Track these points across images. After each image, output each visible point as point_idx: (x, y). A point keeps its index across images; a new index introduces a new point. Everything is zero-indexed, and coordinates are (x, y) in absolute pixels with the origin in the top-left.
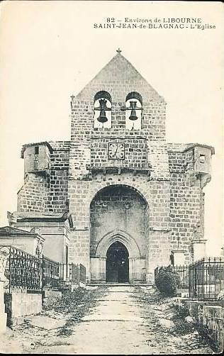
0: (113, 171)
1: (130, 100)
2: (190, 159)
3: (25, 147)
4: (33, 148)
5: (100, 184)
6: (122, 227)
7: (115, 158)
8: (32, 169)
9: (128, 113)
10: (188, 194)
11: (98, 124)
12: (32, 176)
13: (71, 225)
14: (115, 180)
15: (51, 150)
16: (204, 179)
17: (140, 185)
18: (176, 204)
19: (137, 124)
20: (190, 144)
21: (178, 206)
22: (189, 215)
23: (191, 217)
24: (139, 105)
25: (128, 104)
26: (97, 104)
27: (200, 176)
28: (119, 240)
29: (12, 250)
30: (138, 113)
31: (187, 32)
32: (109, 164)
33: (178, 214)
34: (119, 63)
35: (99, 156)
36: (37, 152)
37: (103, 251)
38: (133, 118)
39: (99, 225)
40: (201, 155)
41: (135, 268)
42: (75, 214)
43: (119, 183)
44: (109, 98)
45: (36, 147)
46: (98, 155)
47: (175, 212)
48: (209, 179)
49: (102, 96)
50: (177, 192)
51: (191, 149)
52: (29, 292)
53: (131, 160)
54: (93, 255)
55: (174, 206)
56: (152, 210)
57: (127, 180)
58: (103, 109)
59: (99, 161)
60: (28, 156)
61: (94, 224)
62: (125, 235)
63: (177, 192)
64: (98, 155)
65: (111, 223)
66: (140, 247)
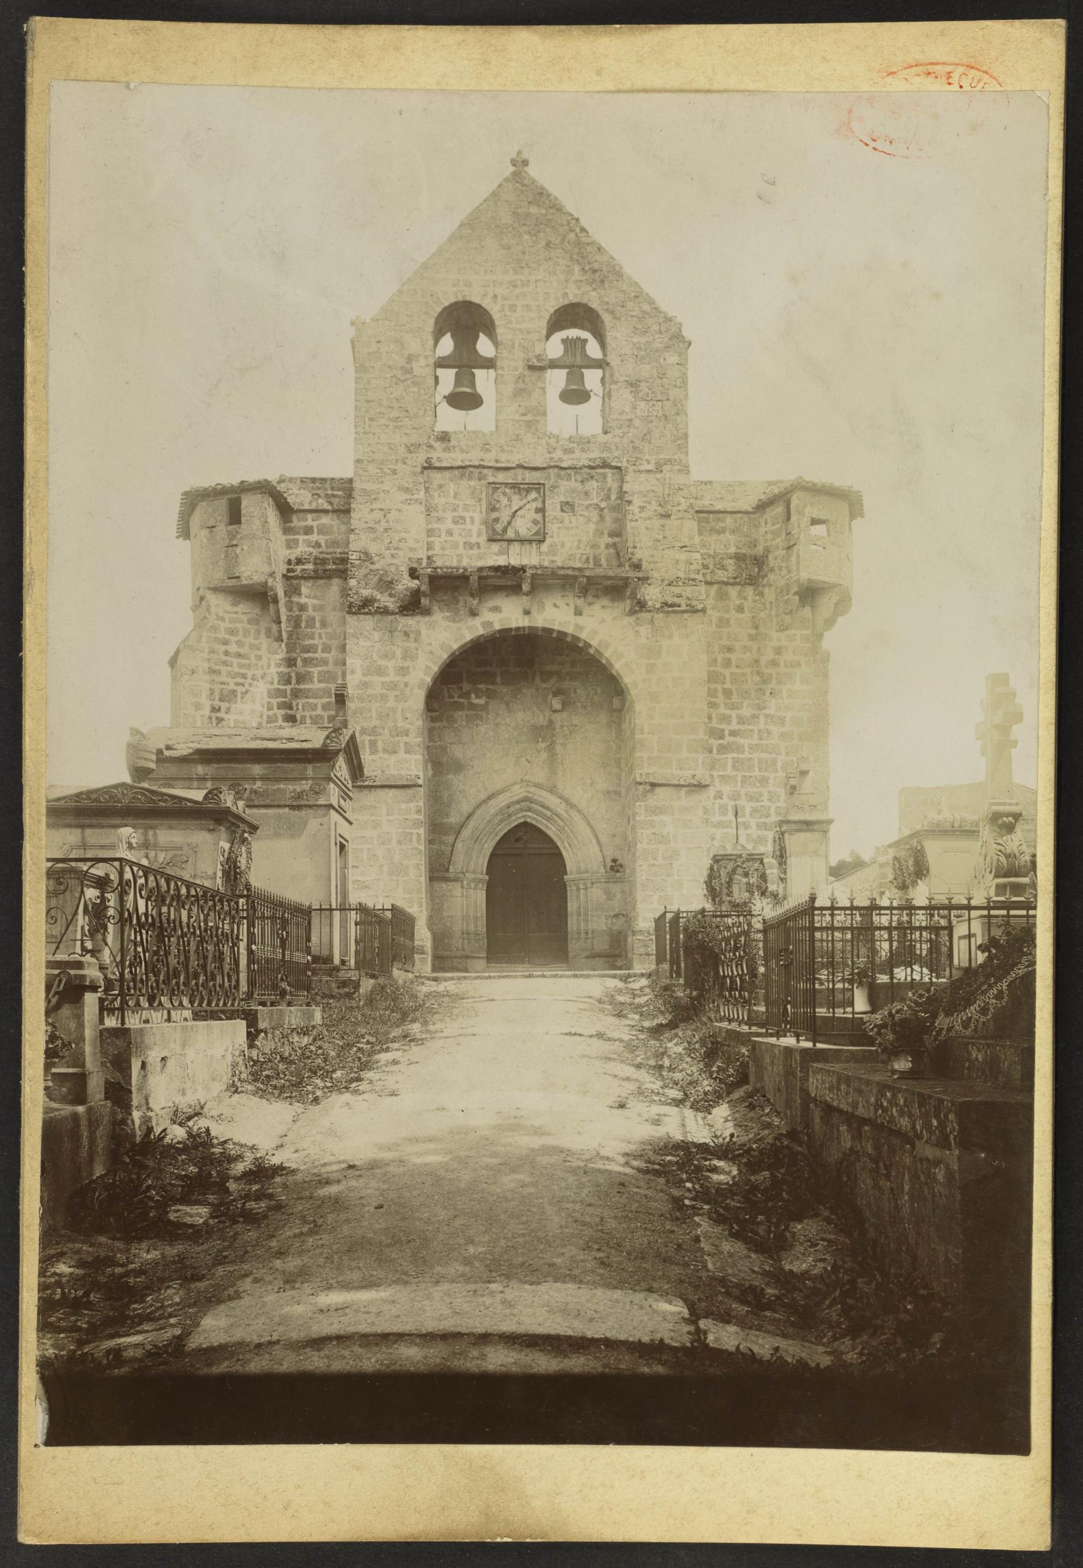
0: (507, 581)
1: (573, 333)
2: (776, 534)
3: (193, 499)
4: (222, 504)
5: (444, 634)
6: (539, 774)
7: (510, 534)
8: (219, 576)
9: (557, 379)
10: (770, 655)
11: (450, 419)
12: (220, 604)
13: (357, 770)
14: (507, 614)
15: (285, 510)
16: (826, 604)
17: (598, 626)
18: (728, 693)
19: (587, 418)
20: (774, 483)
21: (735, 698)
22: (776, 730)
23: (782, 736)
24: (593, 349)
25: (554, 348)
26: (447, 345)
27: (810, 593)
28: (531, 818)
29: (128, 875)
30: (592, 378)
31: (581, 980)
32: (494, 557)
33: (734, 726)
34: (528, 211)
35: (456, 529)
36: (235, 516)
37: (473, 857)
38: (575, 395)
39: (459, 767)
40: (815, 522)
41: (587, 907)
42: (374, 731)
43: (523, 622)
44: (488, 327)
45: (231, 502)
46: (449, 524)
47: (725, 719)
48: (843, 605)
49: (465, 321)
50: (730, 649)
51: (778, 501)
52: (197, 1016)
53: (572, 541)
54: (439, 871)
55: (720, 699)
56: (646, 713)
57: (555, 614)
58: (466, 362)
59: (455, 546)
60: (205, 532)
61: (440, 763)
62: (553, 801)
63: (730, 649)
64: (449, 524)
65: (506, 765)
66: (604, 839)
